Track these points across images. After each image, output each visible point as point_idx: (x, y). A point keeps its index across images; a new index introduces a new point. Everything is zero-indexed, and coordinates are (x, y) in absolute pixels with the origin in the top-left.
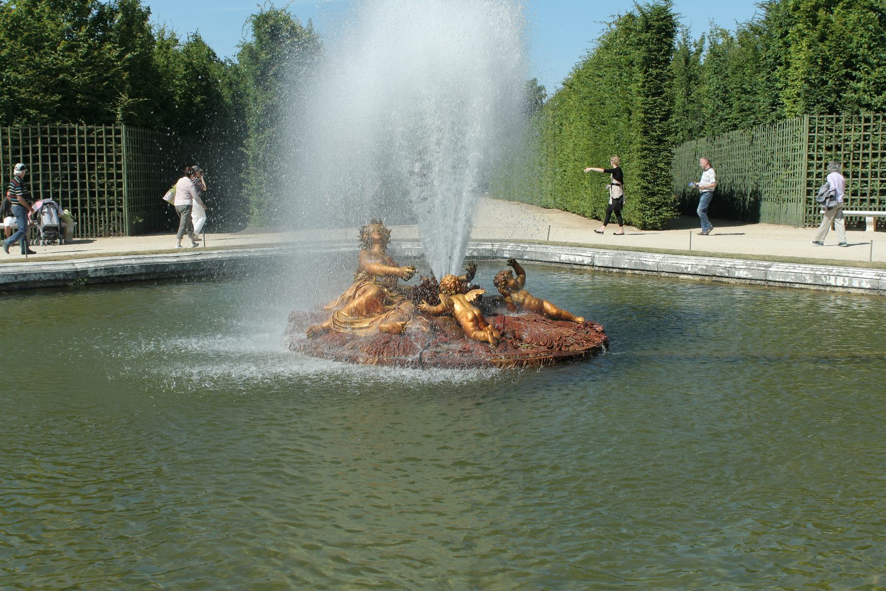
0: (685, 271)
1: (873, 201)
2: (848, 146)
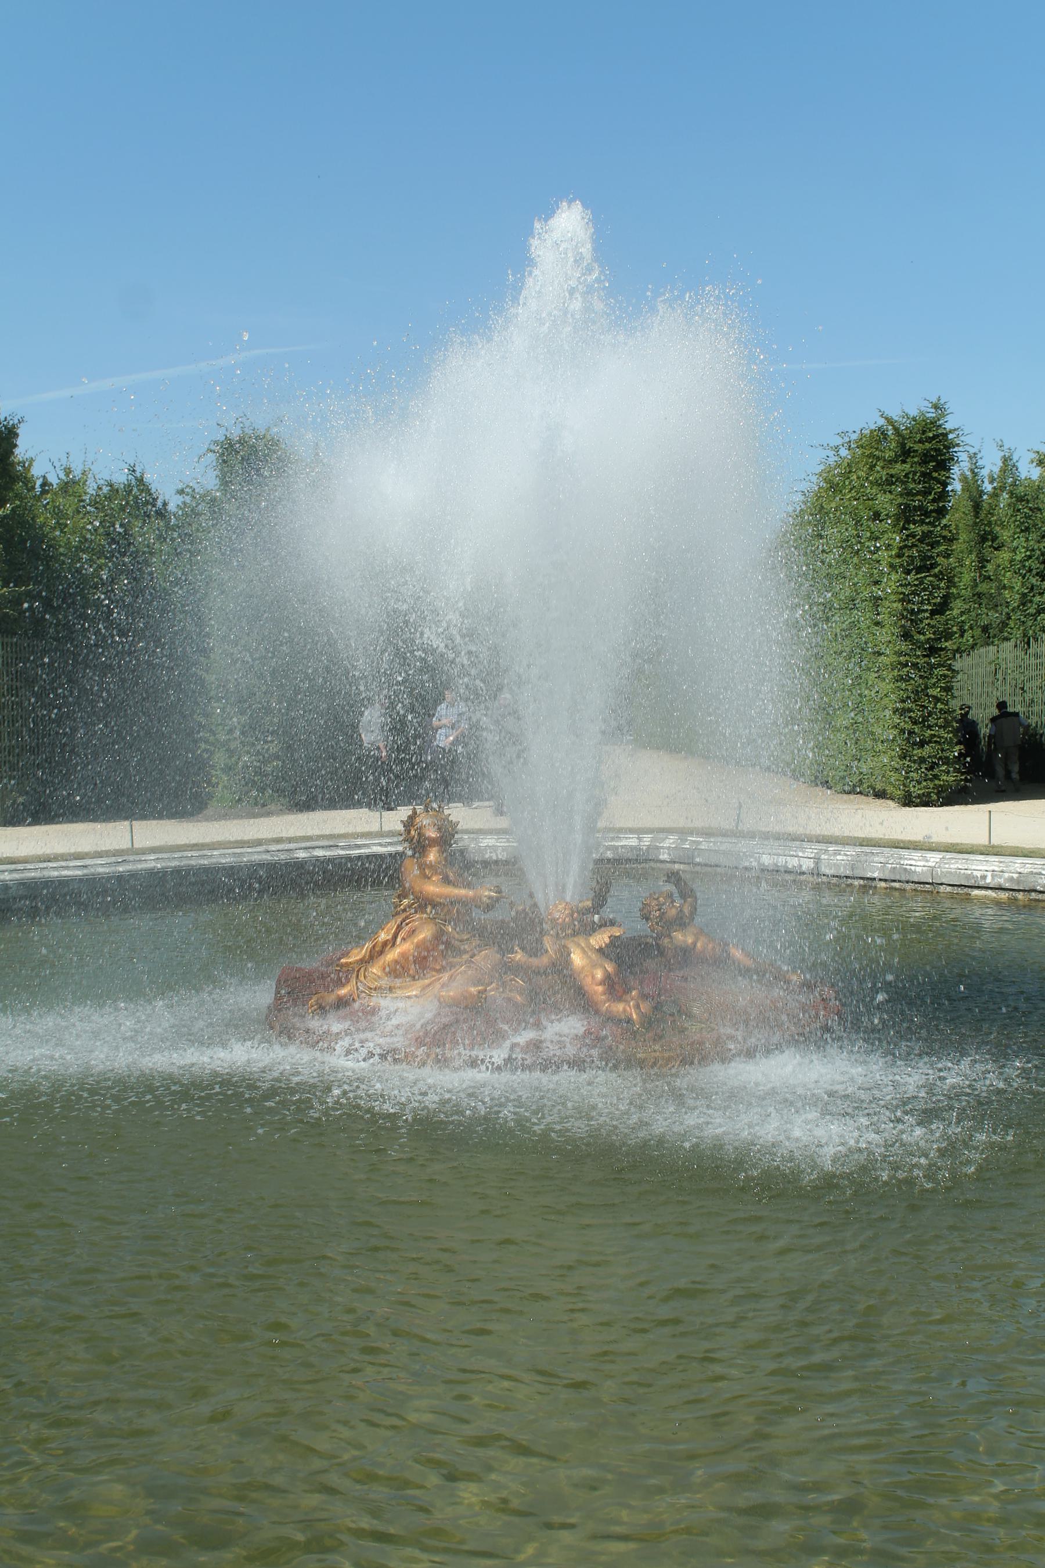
0: (982, 883)
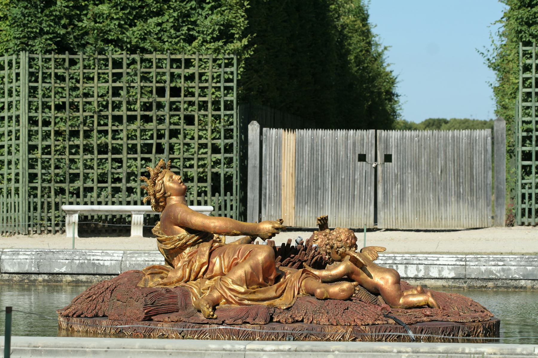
1: (130, 190)
2: (90, 103)
